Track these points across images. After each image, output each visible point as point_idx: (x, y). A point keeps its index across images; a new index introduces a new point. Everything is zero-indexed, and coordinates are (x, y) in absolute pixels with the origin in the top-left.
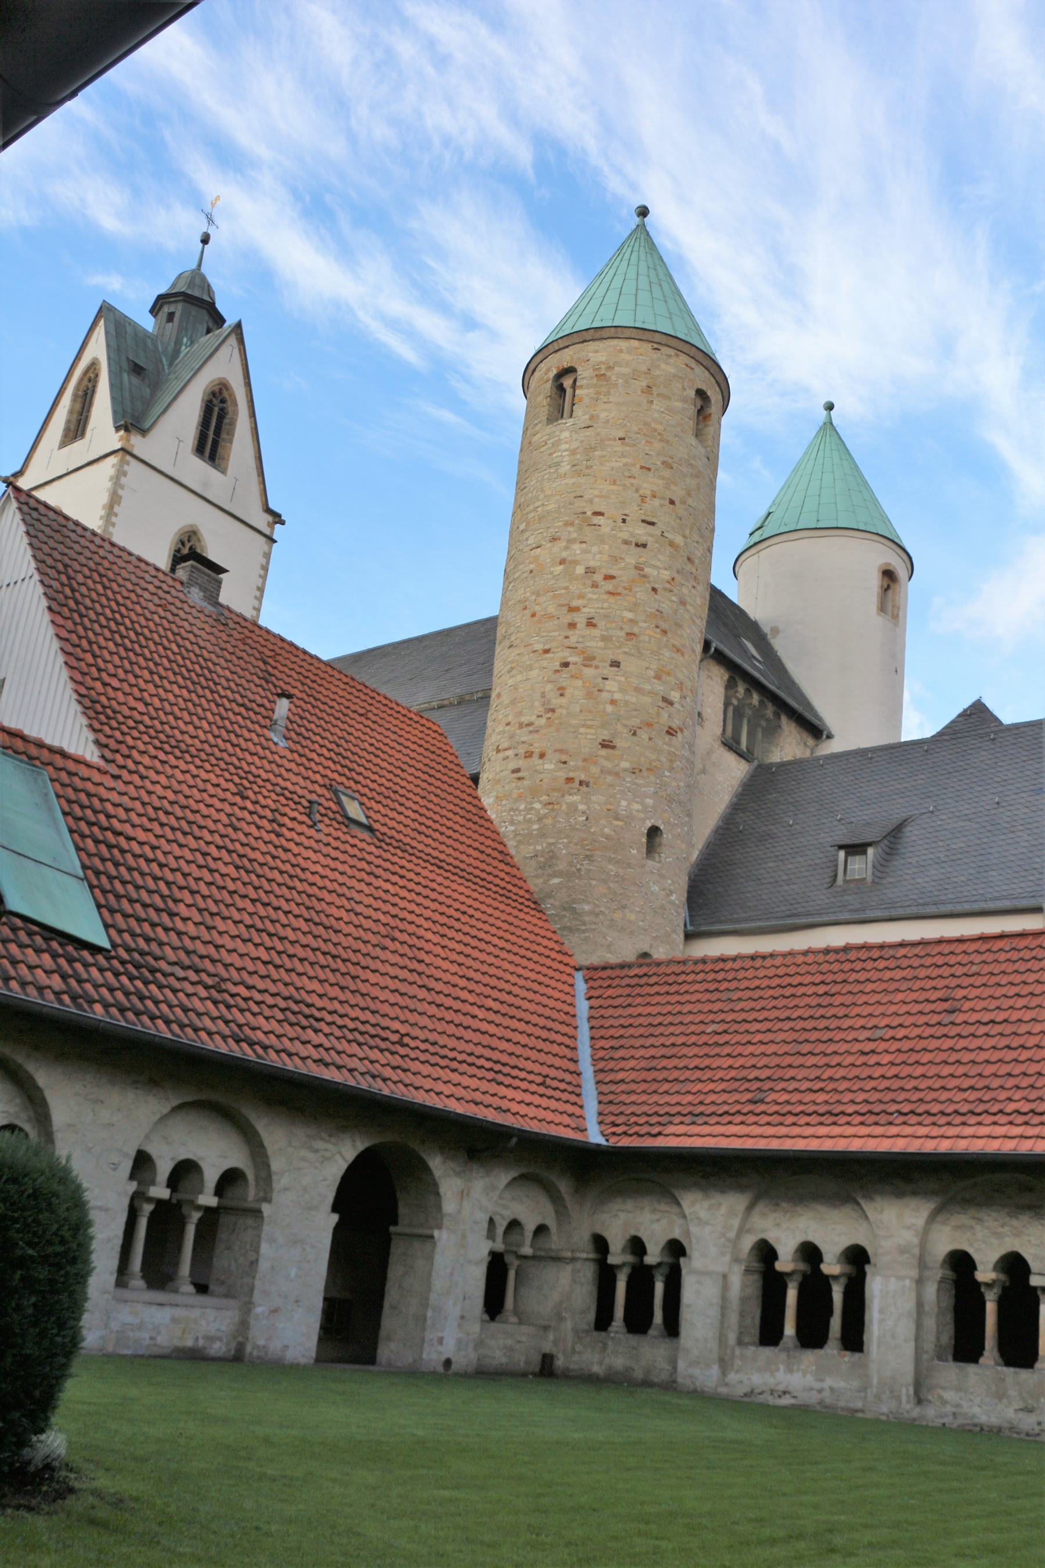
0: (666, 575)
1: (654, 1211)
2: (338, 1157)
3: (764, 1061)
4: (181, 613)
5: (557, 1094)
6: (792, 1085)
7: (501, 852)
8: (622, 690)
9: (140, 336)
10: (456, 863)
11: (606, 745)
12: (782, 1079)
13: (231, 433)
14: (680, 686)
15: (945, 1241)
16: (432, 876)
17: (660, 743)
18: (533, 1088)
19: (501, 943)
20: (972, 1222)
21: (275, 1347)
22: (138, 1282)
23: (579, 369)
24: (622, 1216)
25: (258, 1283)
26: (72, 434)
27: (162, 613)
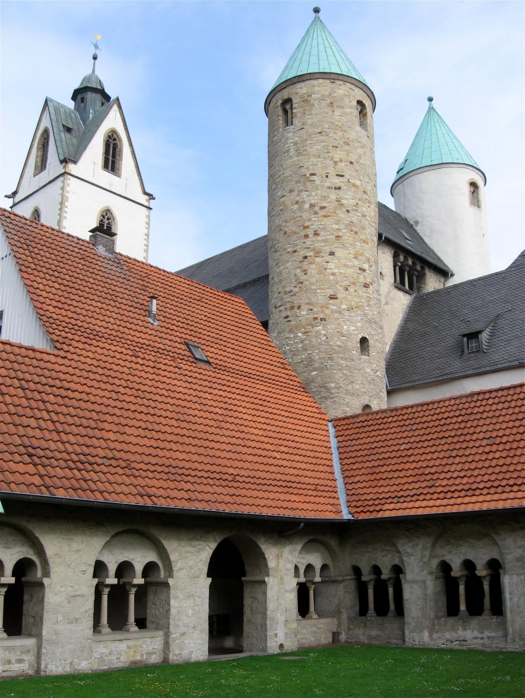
0: (354, 202)
1: (383, 551)
2: (207, 548)
4: (94, 261)
5: (324, 494)
6: (449, 475)
8: (336, 267)
10: (258, 373)
11: (333, 297)
13: (121, 155)
14: (368, 260)
16: (245, 383)
17: (361, 292)
18: (310, 493)
19: (286, 414)
22: (106, 629)
23: (293, 99)
24: (367, 555)
25: (171, 621)
26: (40, 168)
27: (83, 263)
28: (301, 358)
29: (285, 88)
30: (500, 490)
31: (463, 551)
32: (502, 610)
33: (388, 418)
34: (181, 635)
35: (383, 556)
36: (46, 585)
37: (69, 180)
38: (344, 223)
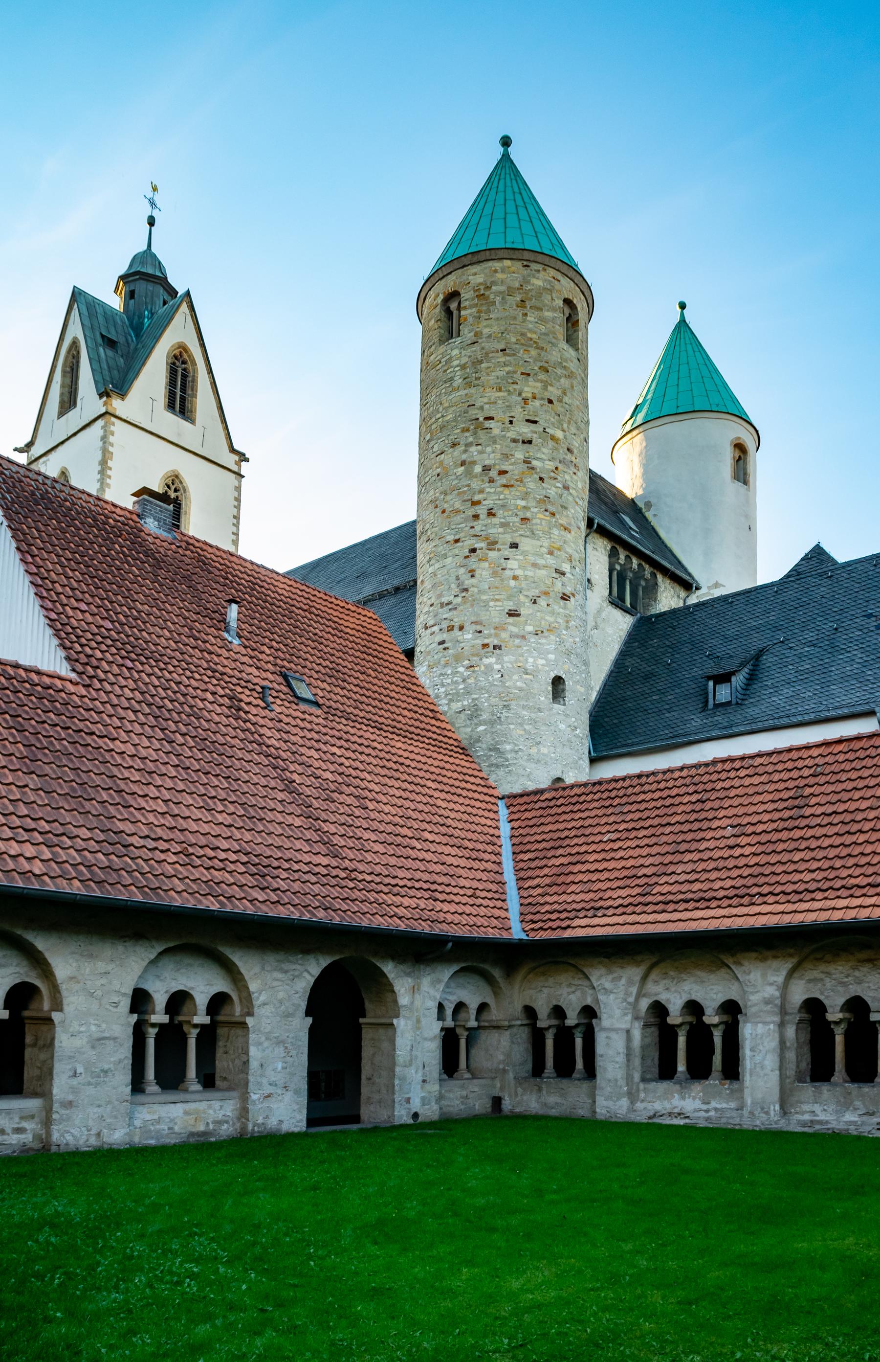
0: (550, 465)
1: (570, 985)
2: (306, 974)
3: (651, 860)
5: (485, 902)
7: (432, 711)
8: (520, 567)
9: (108, 312)
11: (512, 614)
12: (665, 874)
13: (194, 389)
15: (799, 993)
16: (372, 737)
17: (556, 607)
18: (465, 900)
20: (822, 976)
21: (272, 1123)
22: (153, 1087)
23: (462, 292)
24: (546, 990)
25: (251, 1078)
28: (463, 706)
29: (450, 273)
30: (746, 900)
31: (686, 988)
33: (588, 795)
34: (266, 1097)
35: (569, 993)
36: (56, 1022)
37: (113, 424)
38: (535, 498)
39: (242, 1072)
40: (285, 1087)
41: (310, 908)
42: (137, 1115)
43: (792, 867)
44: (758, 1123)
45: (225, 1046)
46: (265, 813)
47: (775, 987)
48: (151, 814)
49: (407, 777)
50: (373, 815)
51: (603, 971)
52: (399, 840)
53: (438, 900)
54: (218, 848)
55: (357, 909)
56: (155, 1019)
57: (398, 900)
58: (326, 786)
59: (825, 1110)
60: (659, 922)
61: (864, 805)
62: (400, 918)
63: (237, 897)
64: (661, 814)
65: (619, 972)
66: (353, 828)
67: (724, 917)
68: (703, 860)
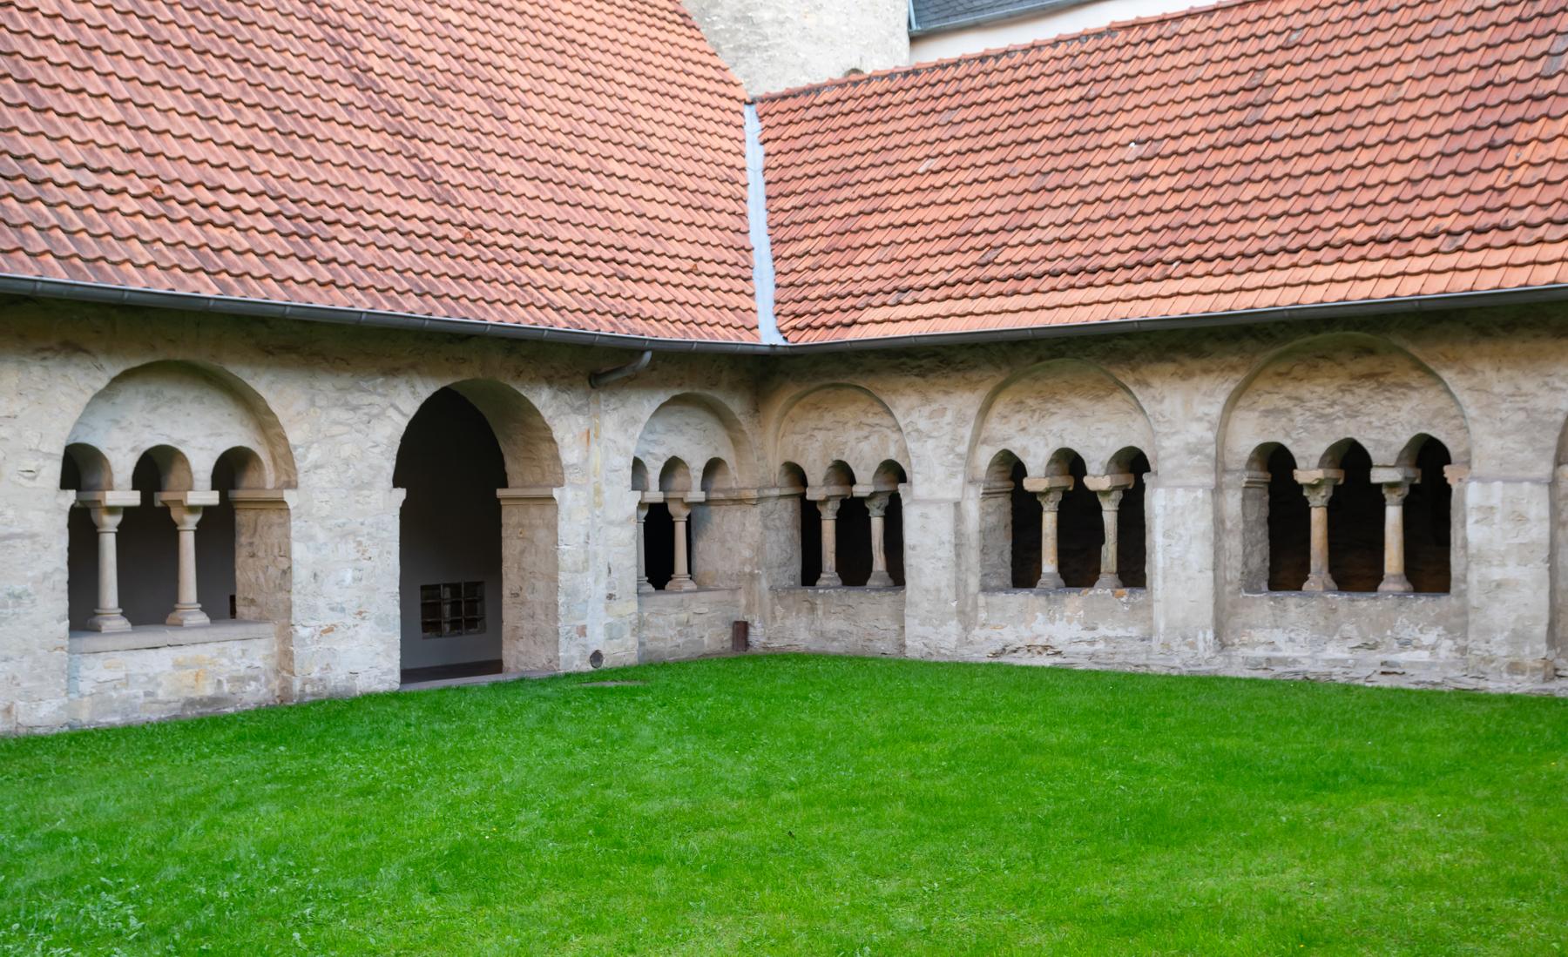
1: (860, 425)
2: (391, 412)
3: (997, 204)
5: (714, 283)
12: (1020, 228)
15: (1248, 435)
18: (677, 278)
20: (1289, 404)
21: (338, 679)
24: (820, 435)
30: (1156, 272)
31: (1055, 428)
32: (1144, 576)
34: (325, 631)
35: (858, 440)
39: (281, 589)
40: (360, 613)
41: (393, 293)
42: (84, 672)
43: (1239, 212)
44: (1177, 662)
45: (251, 544)
46: (315, 126)
47: (1206, 425)
48: (91, 125)
49: (581, 65)
50: (515, 131)
51: (913, 399)
52: (562, 174)
53: (628, 278)
54: (223, 187)
55: (479, 295)
56: (113, 498)
57: (555, 278)
58: (431, 79)
59: (1291, 640)
60: (1007, 311)
61: (1371, 97)
62: (558, 310)
63: (256, 274)
64: (1018, 124)
65: (940, 400)
66: (478, 153)
67: (1118, 300)
68: (1085, 203)
